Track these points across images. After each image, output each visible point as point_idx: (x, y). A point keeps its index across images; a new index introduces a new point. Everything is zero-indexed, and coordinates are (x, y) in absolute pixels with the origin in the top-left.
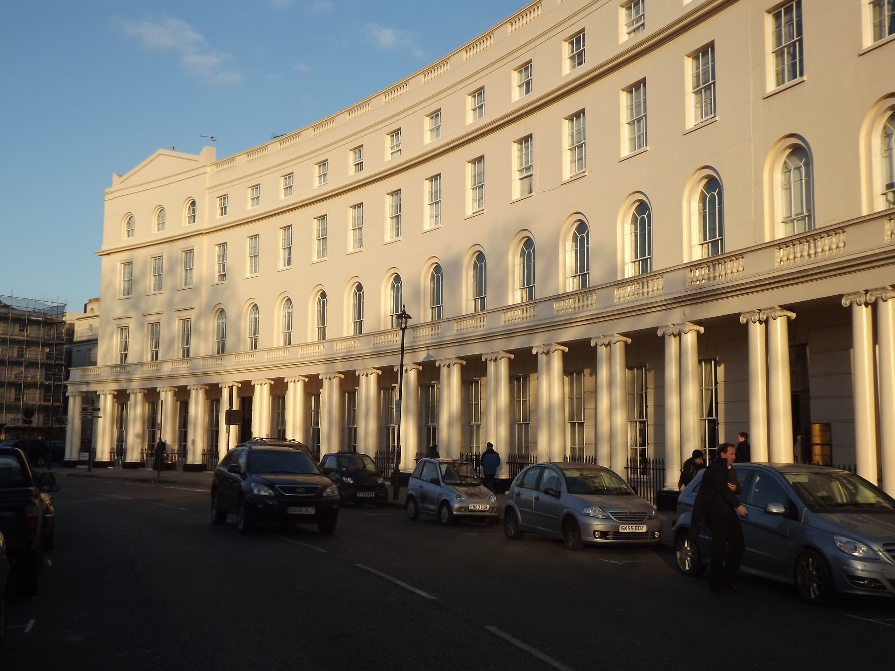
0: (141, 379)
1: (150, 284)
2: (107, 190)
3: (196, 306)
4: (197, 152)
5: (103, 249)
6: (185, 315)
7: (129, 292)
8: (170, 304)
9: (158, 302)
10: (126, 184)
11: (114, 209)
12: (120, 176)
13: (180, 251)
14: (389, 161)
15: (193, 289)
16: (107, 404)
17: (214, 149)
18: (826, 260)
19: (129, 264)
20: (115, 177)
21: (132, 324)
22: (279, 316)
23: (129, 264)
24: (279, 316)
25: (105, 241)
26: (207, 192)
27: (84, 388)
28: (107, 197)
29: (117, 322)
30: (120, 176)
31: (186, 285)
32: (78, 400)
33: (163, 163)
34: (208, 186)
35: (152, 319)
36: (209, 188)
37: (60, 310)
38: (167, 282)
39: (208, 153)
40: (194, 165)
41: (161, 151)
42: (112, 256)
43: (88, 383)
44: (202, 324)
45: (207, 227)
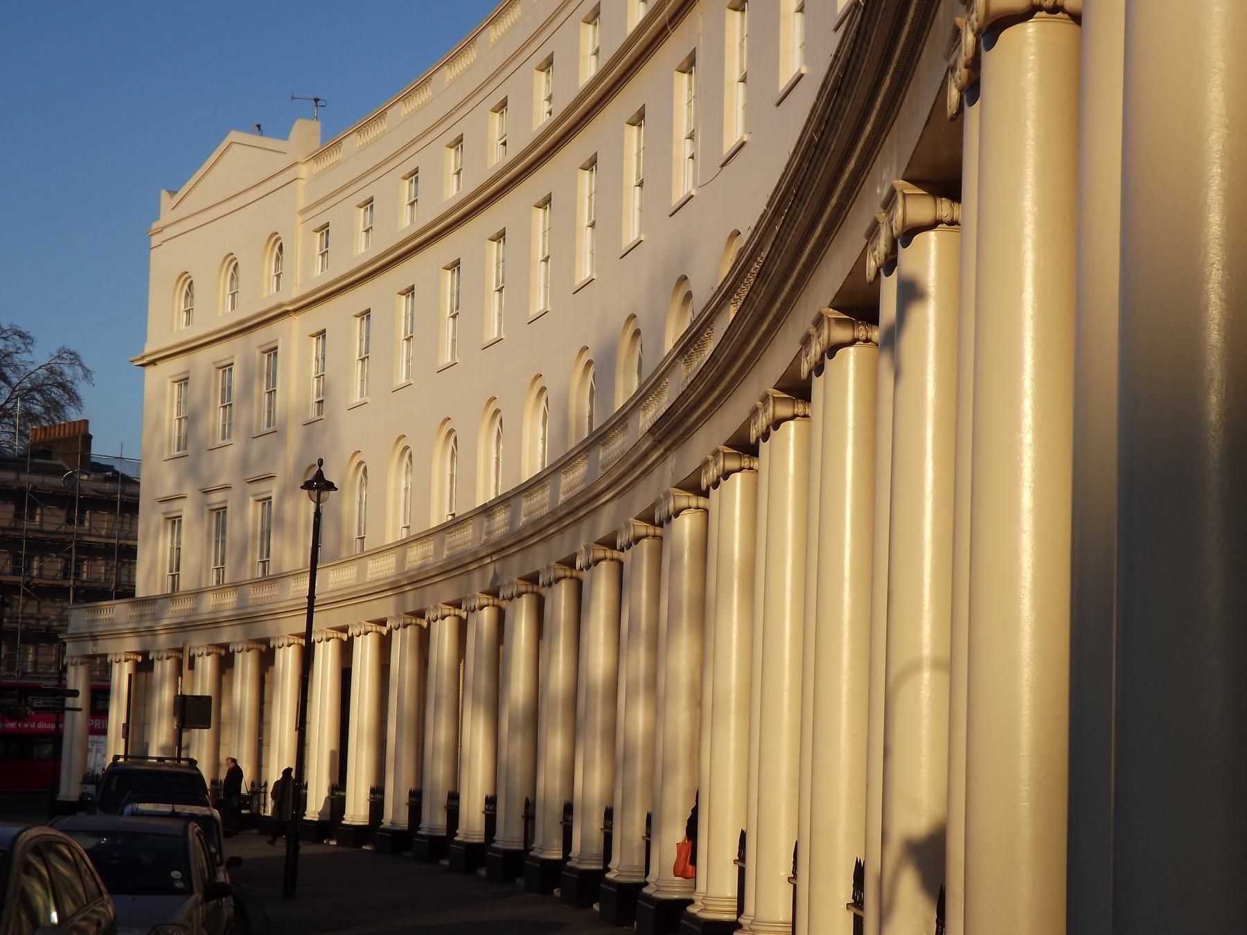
0: (169, 629)
1: (215, 427)
2: (155, 225)
3: (279, 473)
4: (283, 133)
5: (149, 348)
6: (263, 487)
7: (183, 443)
8: (244, 463)
9: (225, 464)
10: (183, 210)
11: (164, 262)
12: (173, 193)
13: (258, 352)
14: (362, 254)
15: (275, 431)
16: (122, 675)
17: (316, 126)
18: (642, 474)
19: (184, 381)
20: (165, 200)
21: (187, 510)
22: (397, 491)
23: (184, 381)
24: (397, 491)
25: (152, 333)
26: (300, 219)
27: (90, 649)
28: (155, 240)
29: (164, 507)
30: (173, 193)
31: (269, 425)
32: (82, 670)
33: (240, 159)
34: (301, 205)
35: (216, 498)
36: (303, 212)
37: (137, 465)
38: (242, 417)
39: (306, 132)
40: (284, 161)
41: (234, 136)
42: (161, 366)
43: (94, 638)
44: (288, 507)
45: (294, 296)
